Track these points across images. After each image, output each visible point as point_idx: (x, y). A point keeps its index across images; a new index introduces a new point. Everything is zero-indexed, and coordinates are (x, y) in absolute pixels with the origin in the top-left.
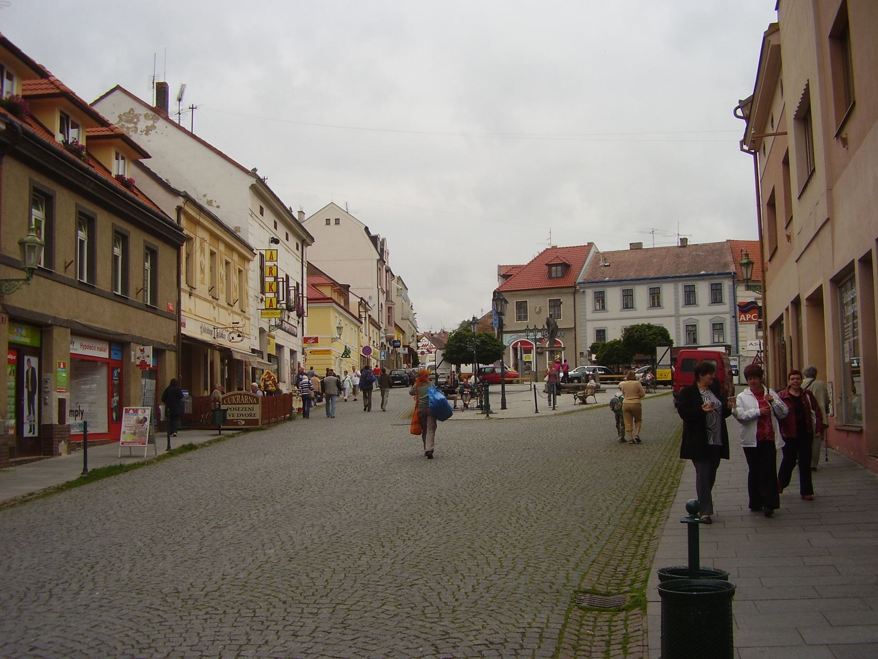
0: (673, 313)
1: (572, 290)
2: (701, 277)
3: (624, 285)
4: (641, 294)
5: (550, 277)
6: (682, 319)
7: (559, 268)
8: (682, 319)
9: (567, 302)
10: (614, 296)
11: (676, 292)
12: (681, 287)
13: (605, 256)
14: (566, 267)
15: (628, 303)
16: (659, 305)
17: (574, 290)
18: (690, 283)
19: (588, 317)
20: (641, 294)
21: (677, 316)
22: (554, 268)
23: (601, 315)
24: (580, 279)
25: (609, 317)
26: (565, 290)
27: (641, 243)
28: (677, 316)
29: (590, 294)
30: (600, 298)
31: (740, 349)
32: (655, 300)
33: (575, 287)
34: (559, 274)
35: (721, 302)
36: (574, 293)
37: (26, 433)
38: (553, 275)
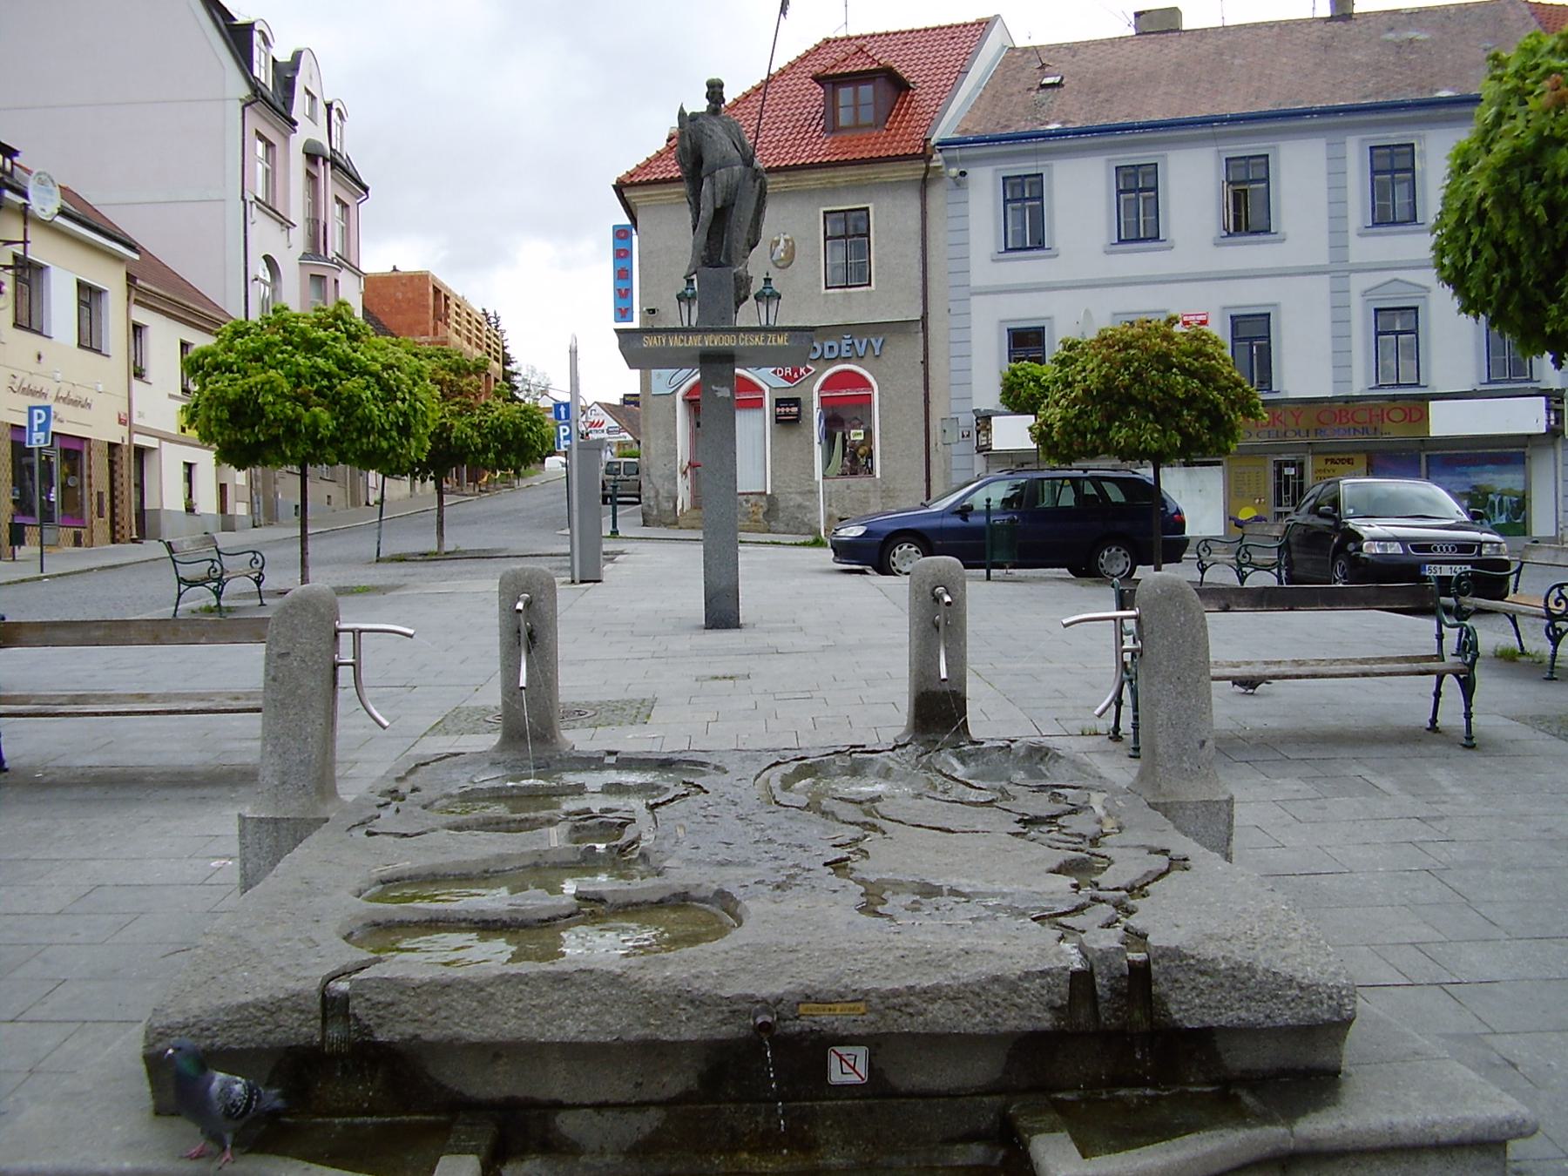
0: (1322, 258)
1: (913, 171)
2: (1431, 109)
3: (833, 190)
4: (1192, 182)
5: (832, 127)
6: (1359, 283)
7: (866, 91)
8: (1359, 283)
9: (891, 218)
10: (1080, 191)
11: (1336, 175)
12: (1355, 151)
13: (1039, 57)
14: (894, 84)
15: (1138, 212)
16: (1039, 244)
17: (923, 168)
18: (1394, 136)
19: (978, 279)
20: (1192, 182)
21: (1339, 270)
22: (845, 94)
23: (1027, 268)
24: (945, 129)
25: (1292, 263)
26: (888, 173)
27: (1174, 13)
28: (1339, 270)
29: (983, 191)
30: (1026, 208)
31: (135, 415)
32: (1247, 212)
33: (926, 157)
34: (867, 116)
35: (1156, 238)
36: (924, 185)
37: (8, 194)
38: (844, 118)
